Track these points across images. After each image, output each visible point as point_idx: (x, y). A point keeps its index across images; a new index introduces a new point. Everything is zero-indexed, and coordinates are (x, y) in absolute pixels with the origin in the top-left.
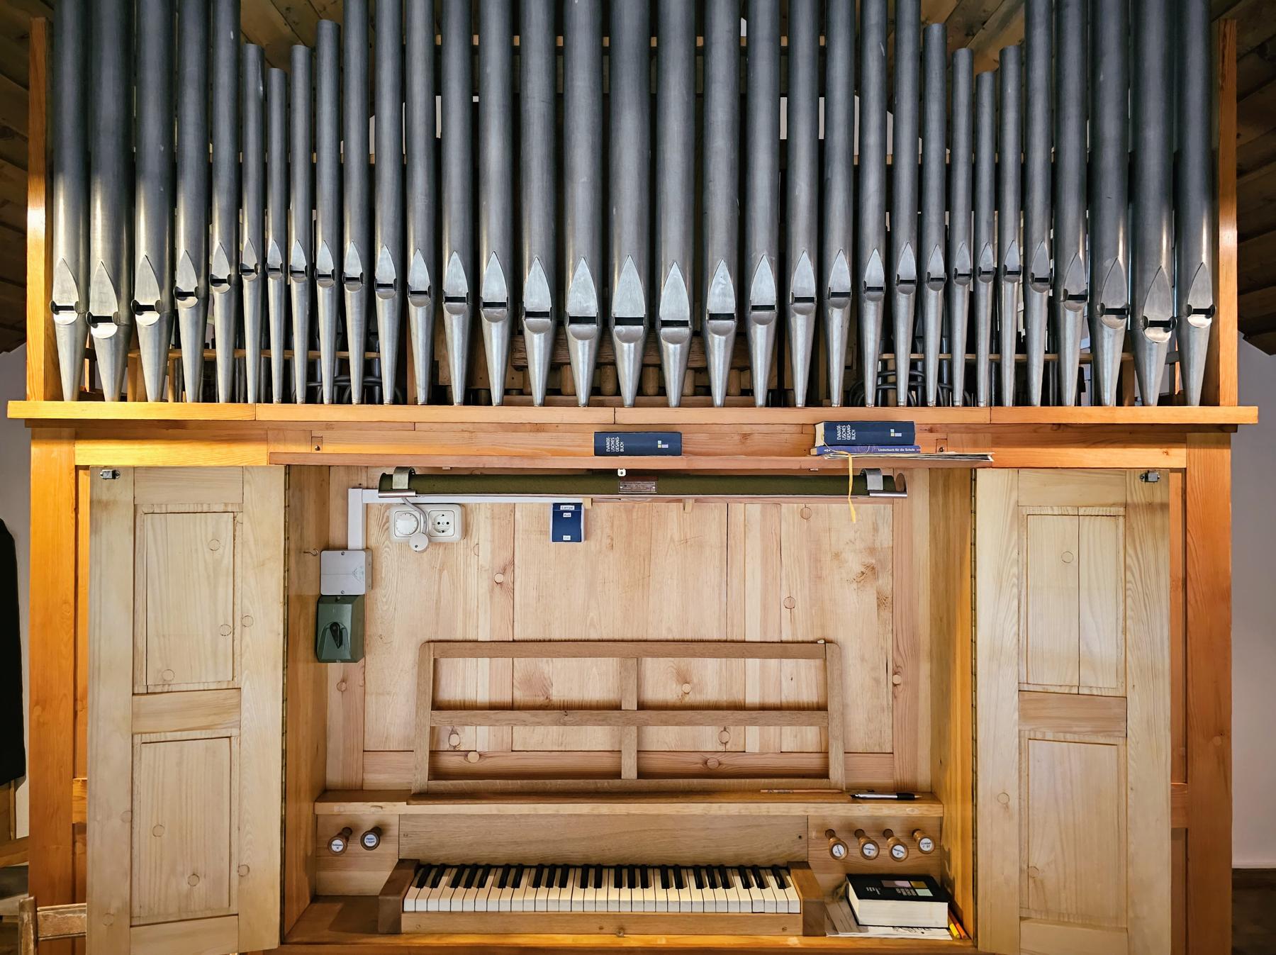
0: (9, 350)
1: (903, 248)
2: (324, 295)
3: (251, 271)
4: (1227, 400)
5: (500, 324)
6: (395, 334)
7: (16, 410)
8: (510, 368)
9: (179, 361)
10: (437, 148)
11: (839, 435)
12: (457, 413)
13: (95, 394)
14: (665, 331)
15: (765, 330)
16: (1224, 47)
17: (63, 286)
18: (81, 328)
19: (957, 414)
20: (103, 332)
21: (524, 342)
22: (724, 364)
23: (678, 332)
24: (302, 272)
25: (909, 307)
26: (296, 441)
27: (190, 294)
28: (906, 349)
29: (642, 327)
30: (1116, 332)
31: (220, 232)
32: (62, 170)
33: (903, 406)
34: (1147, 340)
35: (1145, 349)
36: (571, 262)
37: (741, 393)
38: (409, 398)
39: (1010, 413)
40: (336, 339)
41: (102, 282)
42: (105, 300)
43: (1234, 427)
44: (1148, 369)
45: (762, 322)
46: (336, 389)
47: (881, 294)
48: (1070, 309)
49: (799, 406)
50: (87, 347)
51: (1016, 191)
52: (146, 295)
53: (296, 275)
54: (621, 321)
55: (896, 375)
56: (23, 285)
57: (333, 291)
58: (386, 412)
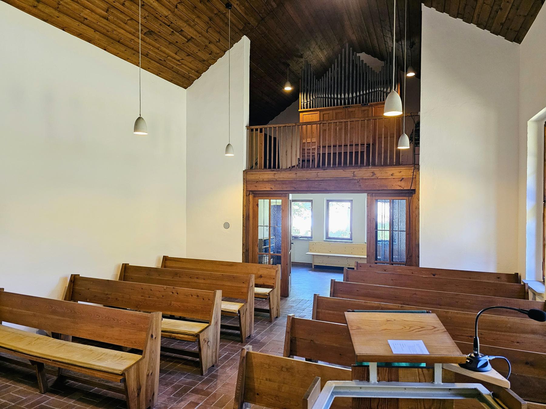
42: (305, 101)
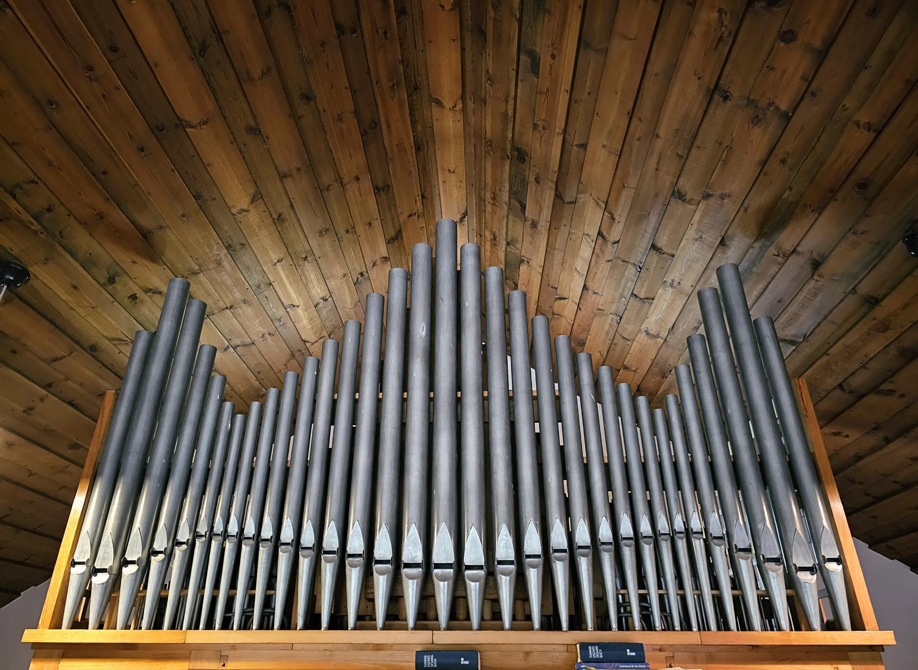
0: (36, 585)
1: (621, 516)
2: (246, 550)
3: (203, 536)
4: (870, 627)
5: (358, 569)
6: (288, 577)
7: (30, 636)
8: (363, 600)
9: (144, 598)
10: (329, 454)
11: (590, 653)
12: (324, 636)
13: (80, 624)
14: (468, 572)
15: (536, 572)
16: (802, 394)
17: (82, 548)
18: (87, 576)
19: (678, 638)
20: (100, 579)
21: (373, 581)
22: (510, 596)
23: (476, 574)
24: (234, 536)
25: (631, 556)
26: (209, 659)
27: (161, 552)
28: (634, 587)
29: (452, 570)
30: (777, 575)
31: (188, 512)
32: (101, 475)
33: (638, 630)
34: (802, 582)
35: (801, 588)
36: (406, 526)
37: (522, 619)
38: (292, 625)
39: (715, 637)
40: (249, 581)
41: (107, 546)
42: (106, 558)
43: (881, 648)
44: (807, 602)
45: (534, 567)
46: (244, 618)
47: (612, 547)
48: (742, 558)
49: (565, 629)
50: (87, 589)
51: (690, 480)
52: (133, 554)
53: (230, 538)
54: (438, 566)
55: (630, 606)
56: (60, 540)
57: (251, 549)
58: (276, 636)
